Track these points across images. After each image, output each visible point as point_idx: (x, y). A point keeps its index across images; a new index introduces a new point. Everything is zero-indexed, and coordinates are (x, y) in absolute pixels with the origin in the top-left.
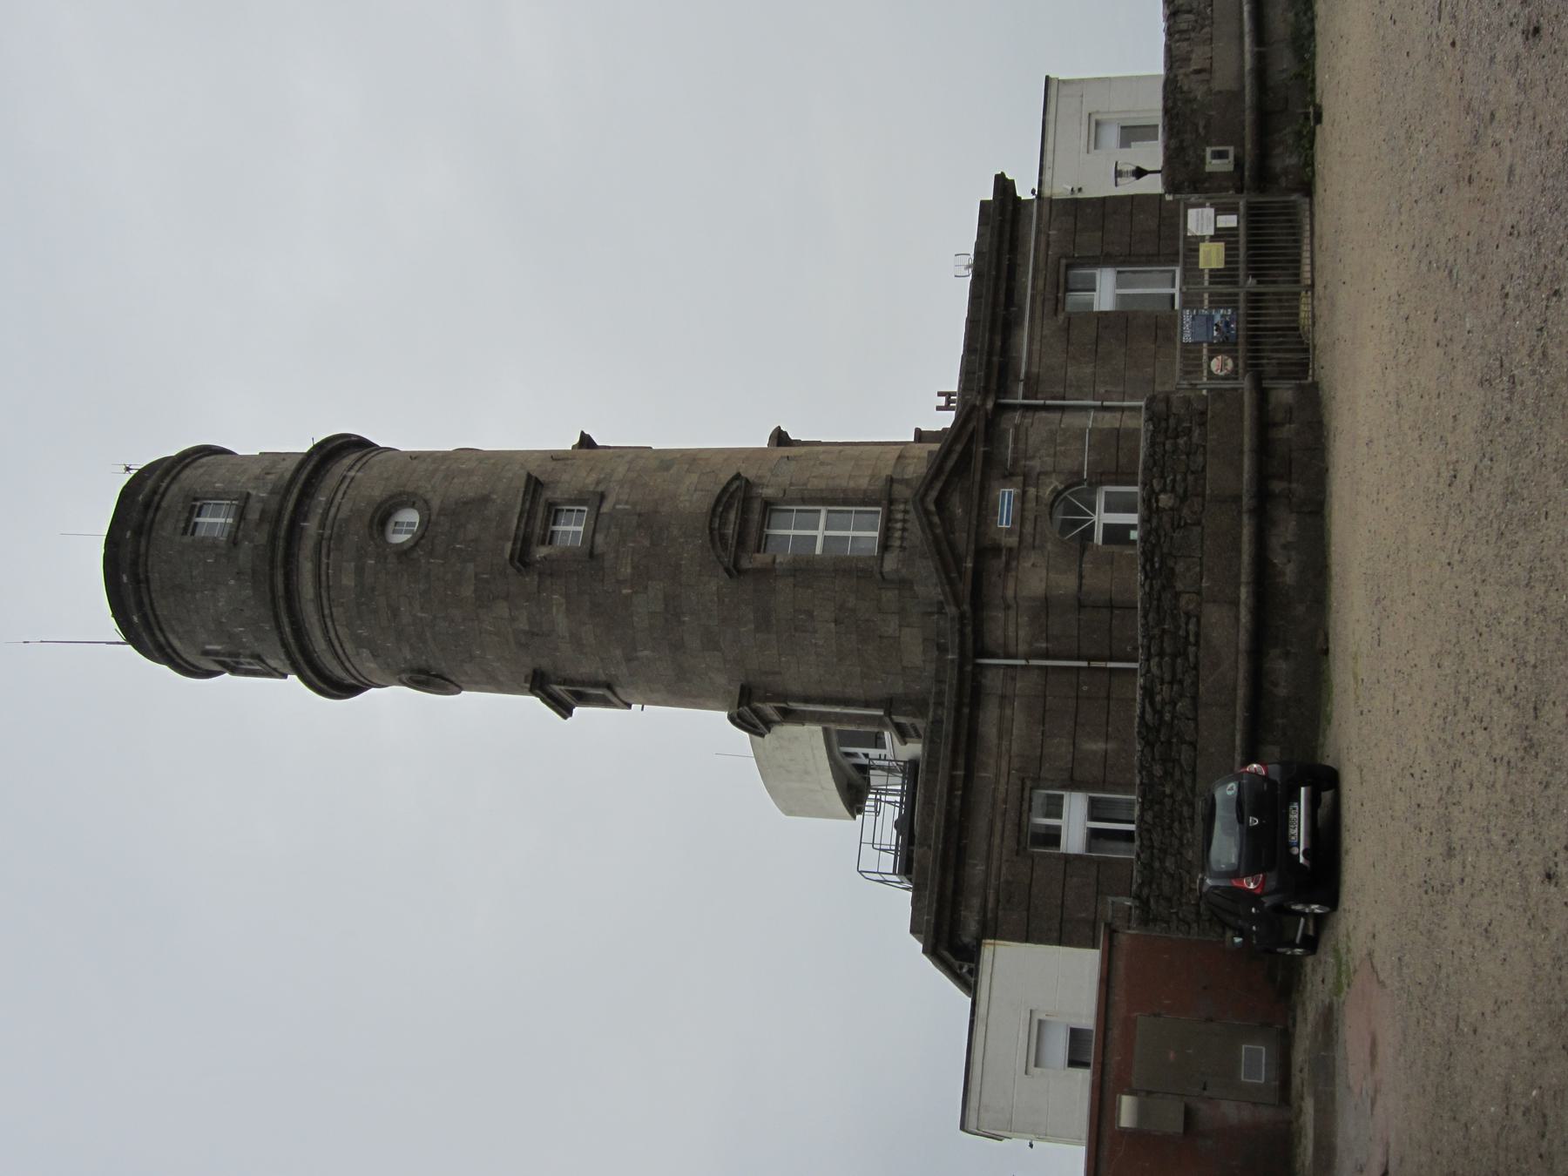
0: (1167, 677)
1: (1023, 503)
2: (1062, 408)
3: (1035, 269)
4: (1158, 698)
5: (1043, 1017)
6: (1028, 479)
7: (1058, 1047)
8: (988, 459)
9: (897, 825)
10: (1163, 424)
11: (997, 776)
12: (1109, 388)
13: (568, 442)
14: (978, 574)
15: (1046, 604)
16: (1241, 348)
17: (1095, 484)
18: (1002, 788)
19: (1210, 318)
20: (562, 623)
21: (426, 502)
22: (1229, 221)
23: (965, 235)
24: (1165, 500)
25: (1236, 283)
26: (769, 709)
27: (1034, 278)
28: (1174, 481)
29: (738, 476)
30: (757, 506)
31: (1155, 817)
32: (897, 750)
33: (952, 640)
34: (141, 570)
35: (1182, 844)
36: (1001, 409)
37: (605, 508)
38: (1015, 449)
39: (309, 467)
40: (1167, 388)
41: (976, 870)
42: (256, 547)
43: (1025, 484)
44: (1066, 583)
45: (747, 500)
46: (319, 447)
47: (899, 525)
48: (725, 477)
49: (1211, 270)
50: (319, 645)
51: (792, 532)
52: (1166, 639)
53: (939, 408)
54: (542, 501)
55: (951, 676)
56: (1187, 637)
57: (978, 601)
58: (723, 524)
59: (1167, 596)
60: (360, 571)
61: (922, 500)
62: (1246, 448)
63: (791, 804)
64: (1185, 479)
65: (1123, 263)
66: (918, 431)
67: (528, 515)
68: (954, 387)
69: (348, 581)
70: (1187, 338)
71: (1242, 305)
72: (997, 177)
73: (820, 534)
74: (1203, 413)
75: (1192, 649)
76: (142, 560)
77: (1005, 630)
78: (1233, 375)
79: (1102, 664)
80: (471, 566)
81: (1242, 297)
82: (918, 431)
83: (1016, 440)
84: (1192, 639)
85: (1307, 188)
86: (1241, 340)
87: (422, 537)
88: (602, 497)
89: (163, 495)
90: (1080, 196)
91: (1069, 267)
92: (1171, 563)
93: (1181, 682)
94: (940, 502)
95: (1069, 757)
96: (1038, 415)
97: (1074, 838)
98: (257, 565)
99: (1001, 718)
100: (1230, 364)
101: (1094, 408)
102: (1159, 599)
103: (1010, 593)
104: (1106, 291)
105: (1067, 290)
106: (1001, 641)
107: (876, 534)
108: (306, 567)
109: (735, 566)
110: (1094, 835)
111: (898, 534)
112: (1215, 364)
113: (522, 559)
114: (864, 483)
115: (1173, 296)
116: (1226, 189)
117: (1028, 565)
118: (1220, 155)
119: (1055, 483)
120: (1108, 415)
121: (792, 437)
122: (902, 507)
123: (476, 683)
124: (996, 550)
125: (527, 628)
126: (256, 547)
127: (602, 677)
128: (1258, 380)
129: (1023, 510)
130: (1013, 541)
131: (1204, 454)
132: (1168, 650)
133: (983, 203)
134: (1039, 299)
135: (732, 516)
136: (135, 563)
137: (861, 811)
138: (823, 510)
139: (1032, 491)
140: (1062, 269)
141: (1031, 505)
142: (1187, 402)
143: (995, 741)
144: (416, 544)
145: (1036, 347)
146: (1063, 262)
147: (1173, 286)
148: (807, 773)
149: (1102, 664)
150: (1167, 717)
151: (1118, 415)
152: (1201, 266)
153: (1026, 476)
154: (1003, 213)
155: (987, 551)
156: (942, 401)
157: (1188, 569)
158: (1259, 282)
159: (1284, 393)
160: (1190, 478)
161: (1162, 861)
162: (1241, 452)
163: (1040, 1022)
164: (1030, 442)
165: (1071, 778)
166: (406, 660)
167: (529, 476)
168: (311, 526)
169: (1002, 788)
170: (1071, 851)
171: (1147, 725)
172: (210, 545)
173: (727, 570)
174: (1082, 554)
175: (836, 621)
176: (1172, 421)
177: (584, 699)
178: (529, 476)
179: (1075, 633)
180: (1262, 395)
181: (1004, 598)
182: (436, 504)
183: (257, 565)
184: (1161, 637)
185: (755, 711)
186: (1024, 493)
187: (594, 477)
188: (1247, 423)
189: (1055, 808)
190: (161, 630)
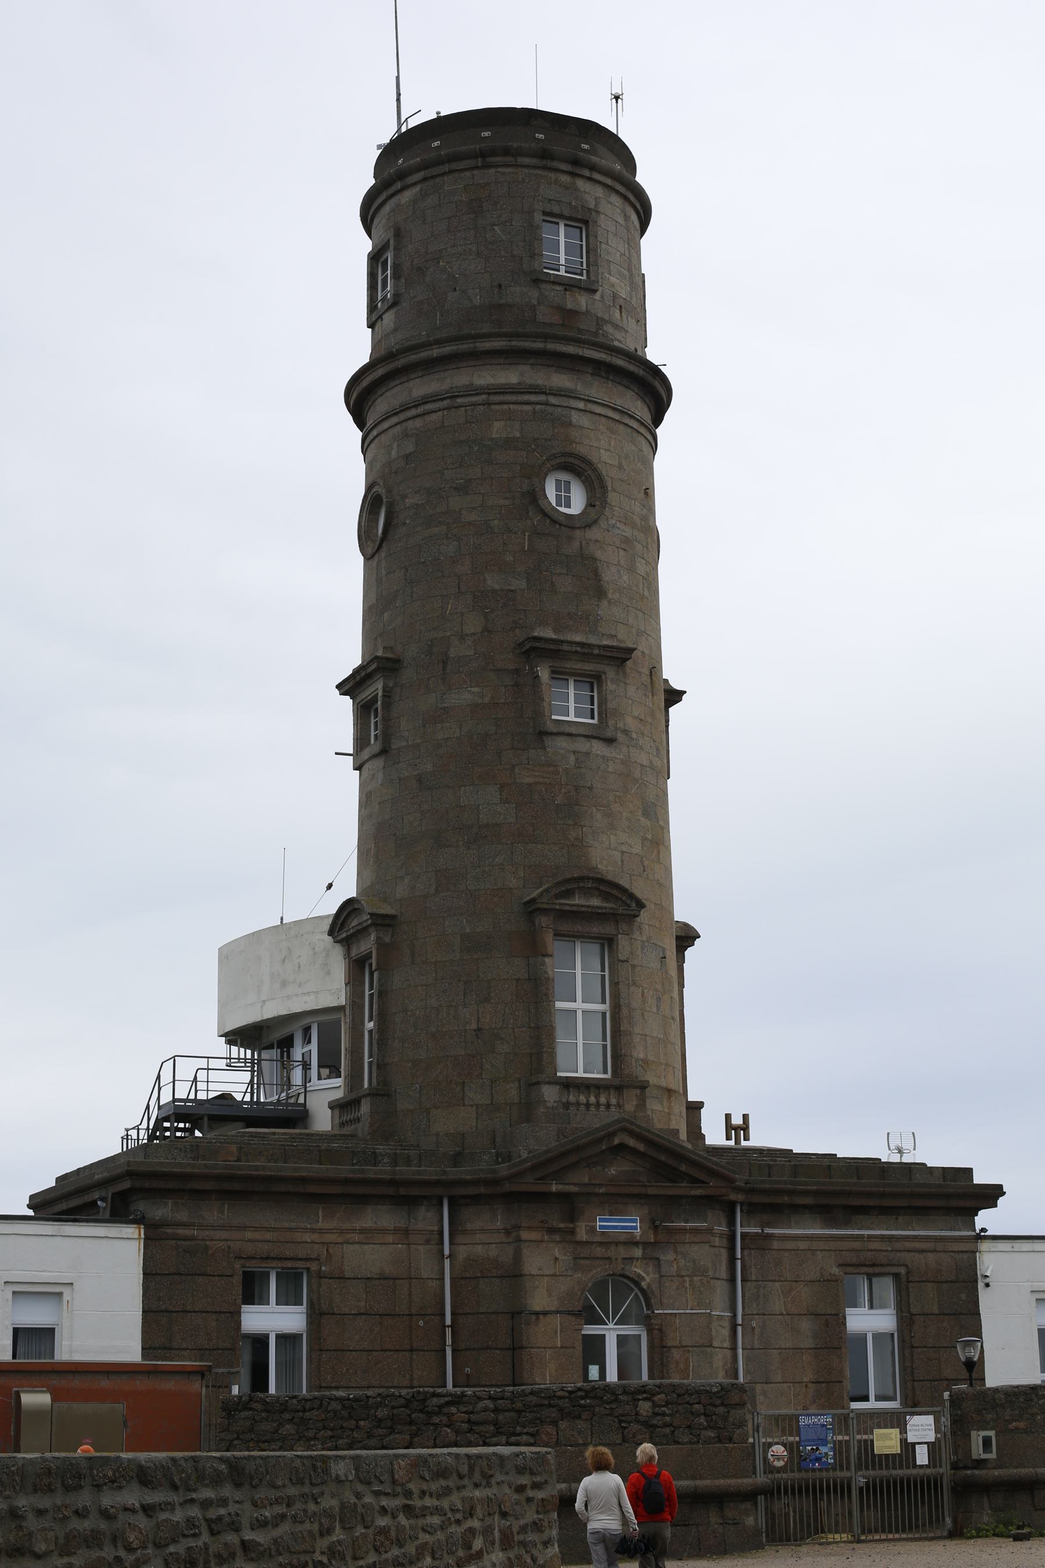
0: (473, 1417)
1: (624, 1243)
2: (732, 1280)
4: (453, 1410)
5: (66, 1297)
6: (651, 1248)
7: (35, 1316)
8: (672, 1201)
9: (225, 1097)
10: (719, 1402)
11: (321, 1231)
12: (757, 1331)
13: (673, 673)
14: (543, 1197)
15: (514, 1275)
16: (796, 1475)
17: (647, 1321)
18: (307, 1237)
19: (824, 1442)
20: (464, 696)
21: (596, 522)
22: (922, 1457)
23: (936, 1153)
24: (645, 1407)
25: (859, 1468)
26: (367, 945)
27: (882, 1238)
28: (664, 1414)
29: (641, 905)
30: (608, 929)
31: (335, 1412)
32: (322, 1096)
33: (464, 1172)
34: (498, 159)
35: (309, 1439)
36: (730, 1209)
37: (598, 748)
38: (683, 1230)
39: (632, 368)
40: (760, 1398)
41: (213, 1214)
42: (533, 308)
43: (646, 1244)
44: (539, 1300)
45: (611, 917)
46: (655, 371)
47: (592, 1099)
48: (639, 889)
49: (872, 1441)
50: (420, 387)
51: (579, 971)
52: (512, 1414)
53: (728, 1117)
54: (607, 669)
55: (429, 1172)
56: (514, 1434)
57: (515, 1199)
58: (587, 892)
59: (553, 1413)
60: (508, 443)
61: (624, 1130)
62: (700, 1483)
63: (237, 959)
64: (666, 1425)
65: (902, 1341)
66: (700, 1105)
67: (586, 652)
68: (759, 1138)
69: (498, 429)
70: (804, 1421)
71: (839, 1474)
72: (1001, 1186)
73: (579, 1005)
74: (730, 1440)
75: (504, 1439)
76: (510, 159)
77: (482, 1230)
78: (769, 1469)
79: (449, 1341)
80: (523, 584)
81: (845, 1474)
82: (700, 1105)
83: (695, 1231)
84: (513, 1439)
85: (957, 1533)
86: (803, 1475)
87: (554, 522)
88: (610, 741)
89: (590, 179)
90: (981, 1285)
91: (896, 1276)
92: (585, 1415)
93: (470, 1430)
94: (622, 1147)
95: (346, 1310)
96: (724, 1253)
98: (503, 295)
99: (383, 1231)
100: (779, 1464)
101: (735, 1316)
102: (550, 1406)
103: (525, 1235)
104: (870, 1320)
105: (870, 1277)
106: (469, 1226)
107: (580, 1074)
108: (510, 376)
109: (538, 909)
110: (260, 1341)
111: (582, 1099)
112: (779, 1449)
113: (535, 650)
114: (639, 1053)
115: (866, 1398)
116: (956, 1453)
117: (557, 1253)
118: (987, 1443)
119: (648, 1278)
120: (726, 1332)
121: (689, 953)
122: (613, 1101)
123: (379, 581)
124: (572, 1217)
125: (452, 654)
126: (533, 308)
127: (396, 744)
128: (770, 1492)
129: (617, 1244)
130: (582, 1235)
131: (690, 1443)
132: (500, 1417)
133: (968, 1172)
134: (856, 1245)
135: (596, 902)
136: (506, 152)
137: (230, 1042)
138: (605, 1007)
139: (638, 1252)
140: (894, 1270)
141: (622, 1252)
142: (742, 1424)
143: (358, 1225)
144: (545, 515)
145: (803, 1245)
146: (902, 1271)
147: (878, 1398)
148: (284, 984)
149: (449, 1341)
150: (436, 1420)
151: (727, 1344)
152: (876, 1431)
154: (959, 1195)
155: (571, 1206)
156: (737, 1120)
157: (580, 1432)
158: (861, 1489)
159: (753, 1519)
160: (667, 1430)
161: (291, 1421)
162: (694, 1478)
163: (60, 1294)
164: (695, 1247)
165: (322, 1314)
166: (404, 497)
167: (631, 650)
168: (561, 380)
169: (307, 1237)
170: (243, 1316)
171: (425, 1400)
172: (533, 245)
173: (533, 901)
174: (569, 1313)
175: (479, 1029)
176: (721, 1410)
177: (363, 712)
178: (631, 650)
179: (483, 1309)
180: (750, 1496)
181: (518, 1227)
182: (594, 534)
183: (503, 295)
184: (513, 1410)
185: (363, 931)
186: (636, 1244)
187: (631, 723)
188: (722, 1482)
189: (288, 1297)
190: (425, 179)
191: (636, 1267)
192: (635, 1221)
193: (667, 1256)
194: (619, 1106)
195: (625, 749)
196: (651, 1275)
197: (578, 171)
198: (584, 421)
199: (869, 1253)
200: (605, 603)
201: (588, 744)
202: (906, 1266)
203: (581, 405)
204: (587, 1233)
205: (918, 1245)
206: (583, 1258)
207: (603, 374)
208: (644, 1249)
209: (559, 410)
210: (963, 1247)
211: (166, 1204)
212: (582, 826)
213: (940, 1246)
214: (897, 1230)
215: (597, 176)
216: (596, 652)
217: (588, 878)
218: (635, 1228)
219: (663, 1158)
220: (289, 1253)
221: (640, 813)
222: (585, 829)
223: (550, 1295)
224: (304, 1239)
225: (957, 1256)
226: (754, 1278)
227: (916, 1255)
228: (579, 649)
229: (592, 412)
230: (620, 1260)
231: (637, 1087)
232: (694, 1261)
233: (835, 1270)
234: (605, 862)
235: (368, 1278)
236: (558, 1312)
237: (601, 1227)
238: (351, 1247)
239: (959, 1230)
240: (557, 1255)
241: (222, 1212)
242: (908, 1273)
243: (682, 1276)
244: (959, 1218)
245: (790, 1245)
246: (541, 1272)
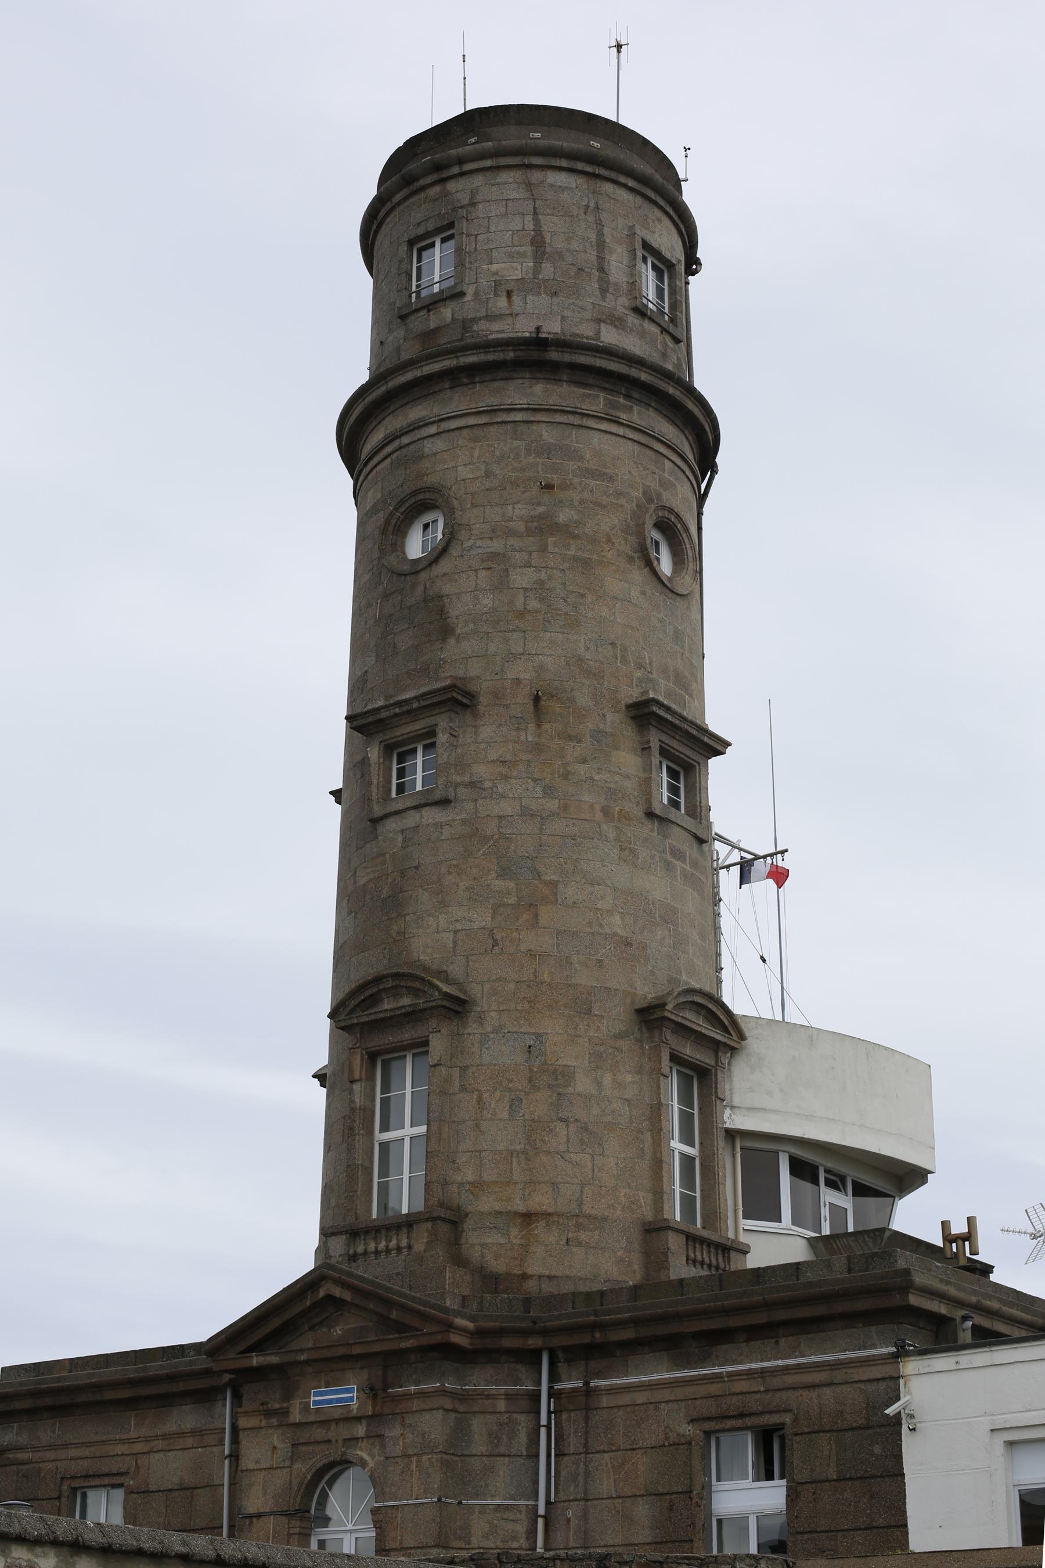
3: (762, 1372)
12: (574, 1523)
18: (119, 1449)
27: (749, 1373)
38: (408, 1396)
41: (48, 1432)
58: (395, 992)
83: (423, 1395)
88: (444, 803)
89: (462, 174)
97: (770, 1497)
130: (296, 1416)
134: (715, 1388)
135: (406, 1001)
139: (361, 1430)
145: (640, 1398)
153: (376, 1417)
156: (959, 1227)
164: (426, 1416)
169: (119, 1449)
186: (358, 1419)
191: (361, 1450)
192: (351, 1391)
193: (394, 1431)
194: (410, 1247)
195: (469, 806)
196: (377, 1458)
197: (444, 174)
198: (439, 444)
199: (735, 1399)
200: (452, 641)
201: (418, 815)
202: (790, 1411)
203: (433, 429)
204: (300, 1413)
205: (790, 1379)
206: (303, 1444)
207: (465, 381)
208: (368, 1425)
209: (412, 446)
210: (877, 1372)
211: (12, 1428)
212: (405, 916)
213: (839, 1376)
214: (776, 1359)
215: (468, 167)
216: (415, 705)
217: (385, 977)
218: (351, 1399)
219: (371, 1306)
220: (105, 1469)
221: (493, 874)
222: (408, 918)
223: (265, 1493)
224: (115, 1453)
225: (871, 1388)
226: (572, 1450)
227: (805, 1393)
228: (397, 710)
229: (448, 431)
230: (340, 1441)
231: (427, 1220)
232: (423, 1435)
233: (688, 1430)
234: (429, 951)
235: (170, 1490)
236: (271, 1513)
237: (316, 1403)
238: (156, 1455)
239: (873, 1346)
240: (275, 1443)
241: (54, 1431)
242: (796, 1420)
243: (410, 1456)
244: (873, 1328)
245: (624, 1399)
246: (258, 1466)
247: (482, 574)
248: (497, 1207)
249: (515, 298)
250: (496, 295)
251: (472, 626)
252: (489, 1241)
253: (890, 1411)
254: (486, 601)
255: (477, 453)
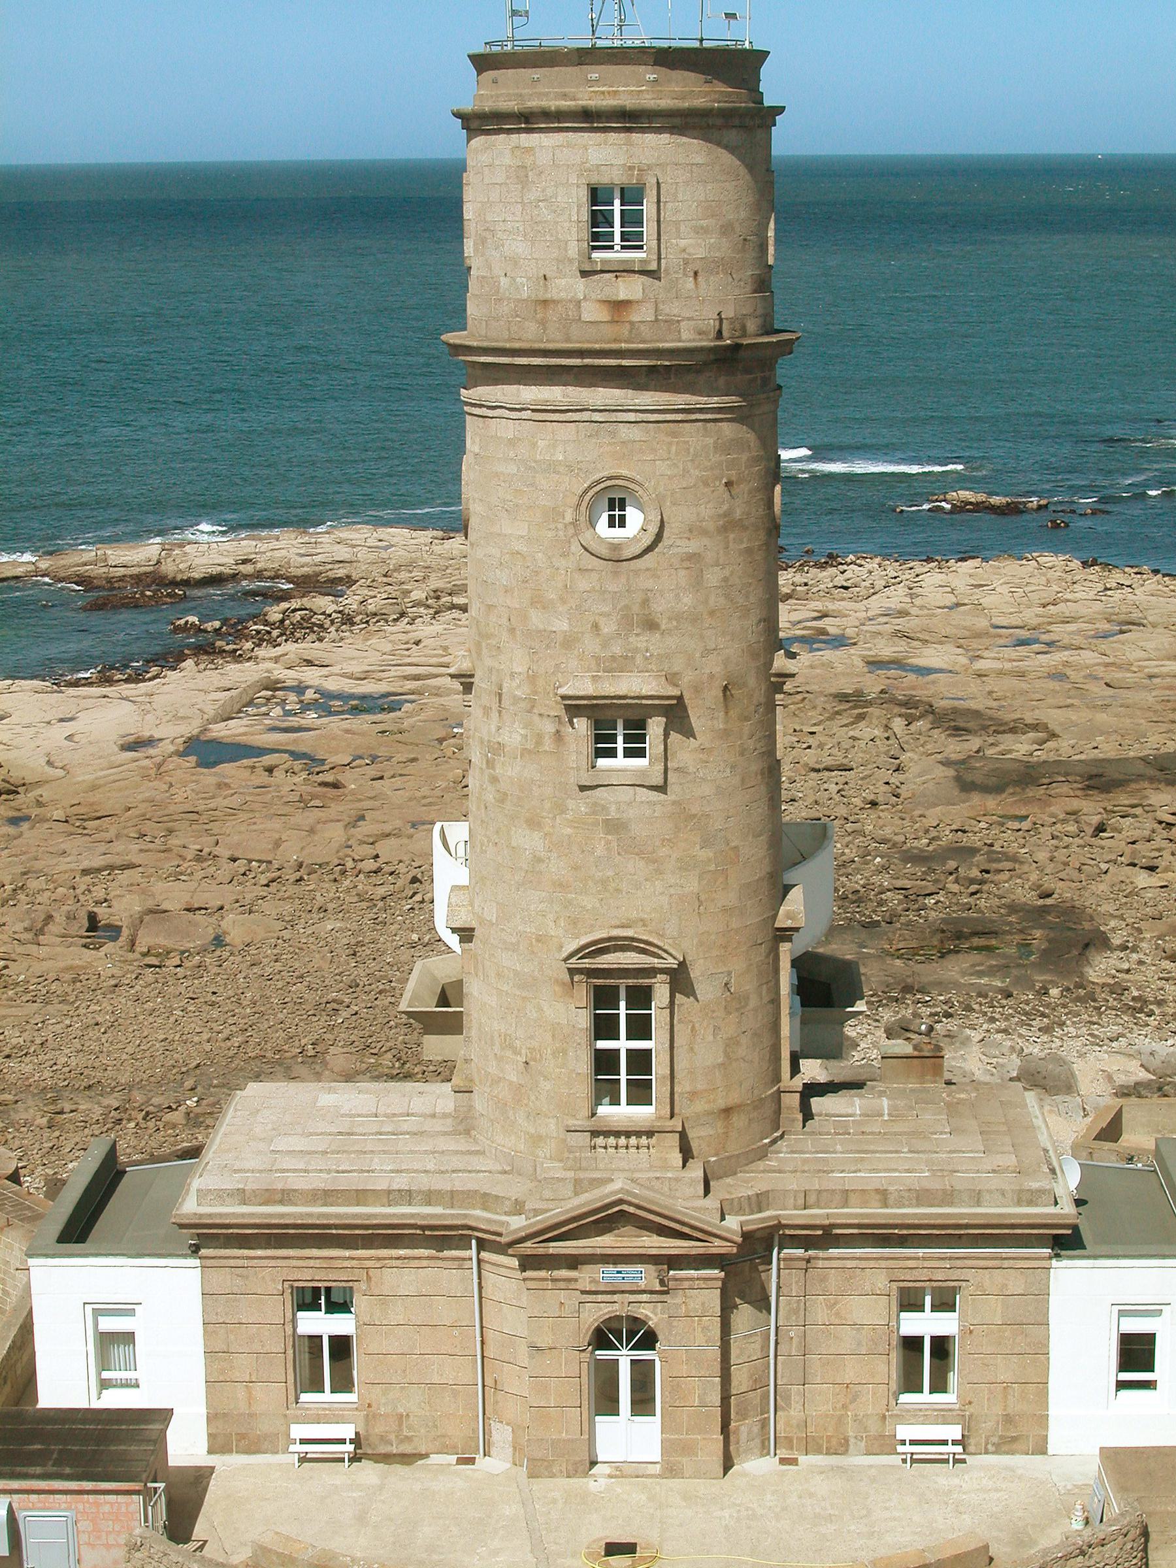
247: (682, 573)
248: (707, 1107)
249: (700, 279)
250: (685, 275)
251: (675, 623)
252: (702, 1134)
253: (738, 1301)
254: (685, 600)
255: (674, 448)
